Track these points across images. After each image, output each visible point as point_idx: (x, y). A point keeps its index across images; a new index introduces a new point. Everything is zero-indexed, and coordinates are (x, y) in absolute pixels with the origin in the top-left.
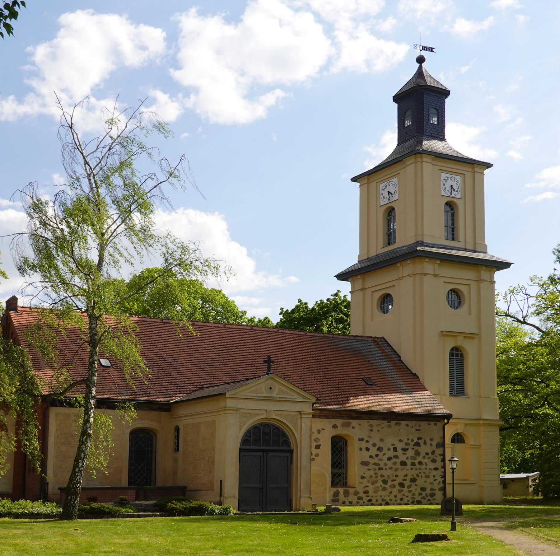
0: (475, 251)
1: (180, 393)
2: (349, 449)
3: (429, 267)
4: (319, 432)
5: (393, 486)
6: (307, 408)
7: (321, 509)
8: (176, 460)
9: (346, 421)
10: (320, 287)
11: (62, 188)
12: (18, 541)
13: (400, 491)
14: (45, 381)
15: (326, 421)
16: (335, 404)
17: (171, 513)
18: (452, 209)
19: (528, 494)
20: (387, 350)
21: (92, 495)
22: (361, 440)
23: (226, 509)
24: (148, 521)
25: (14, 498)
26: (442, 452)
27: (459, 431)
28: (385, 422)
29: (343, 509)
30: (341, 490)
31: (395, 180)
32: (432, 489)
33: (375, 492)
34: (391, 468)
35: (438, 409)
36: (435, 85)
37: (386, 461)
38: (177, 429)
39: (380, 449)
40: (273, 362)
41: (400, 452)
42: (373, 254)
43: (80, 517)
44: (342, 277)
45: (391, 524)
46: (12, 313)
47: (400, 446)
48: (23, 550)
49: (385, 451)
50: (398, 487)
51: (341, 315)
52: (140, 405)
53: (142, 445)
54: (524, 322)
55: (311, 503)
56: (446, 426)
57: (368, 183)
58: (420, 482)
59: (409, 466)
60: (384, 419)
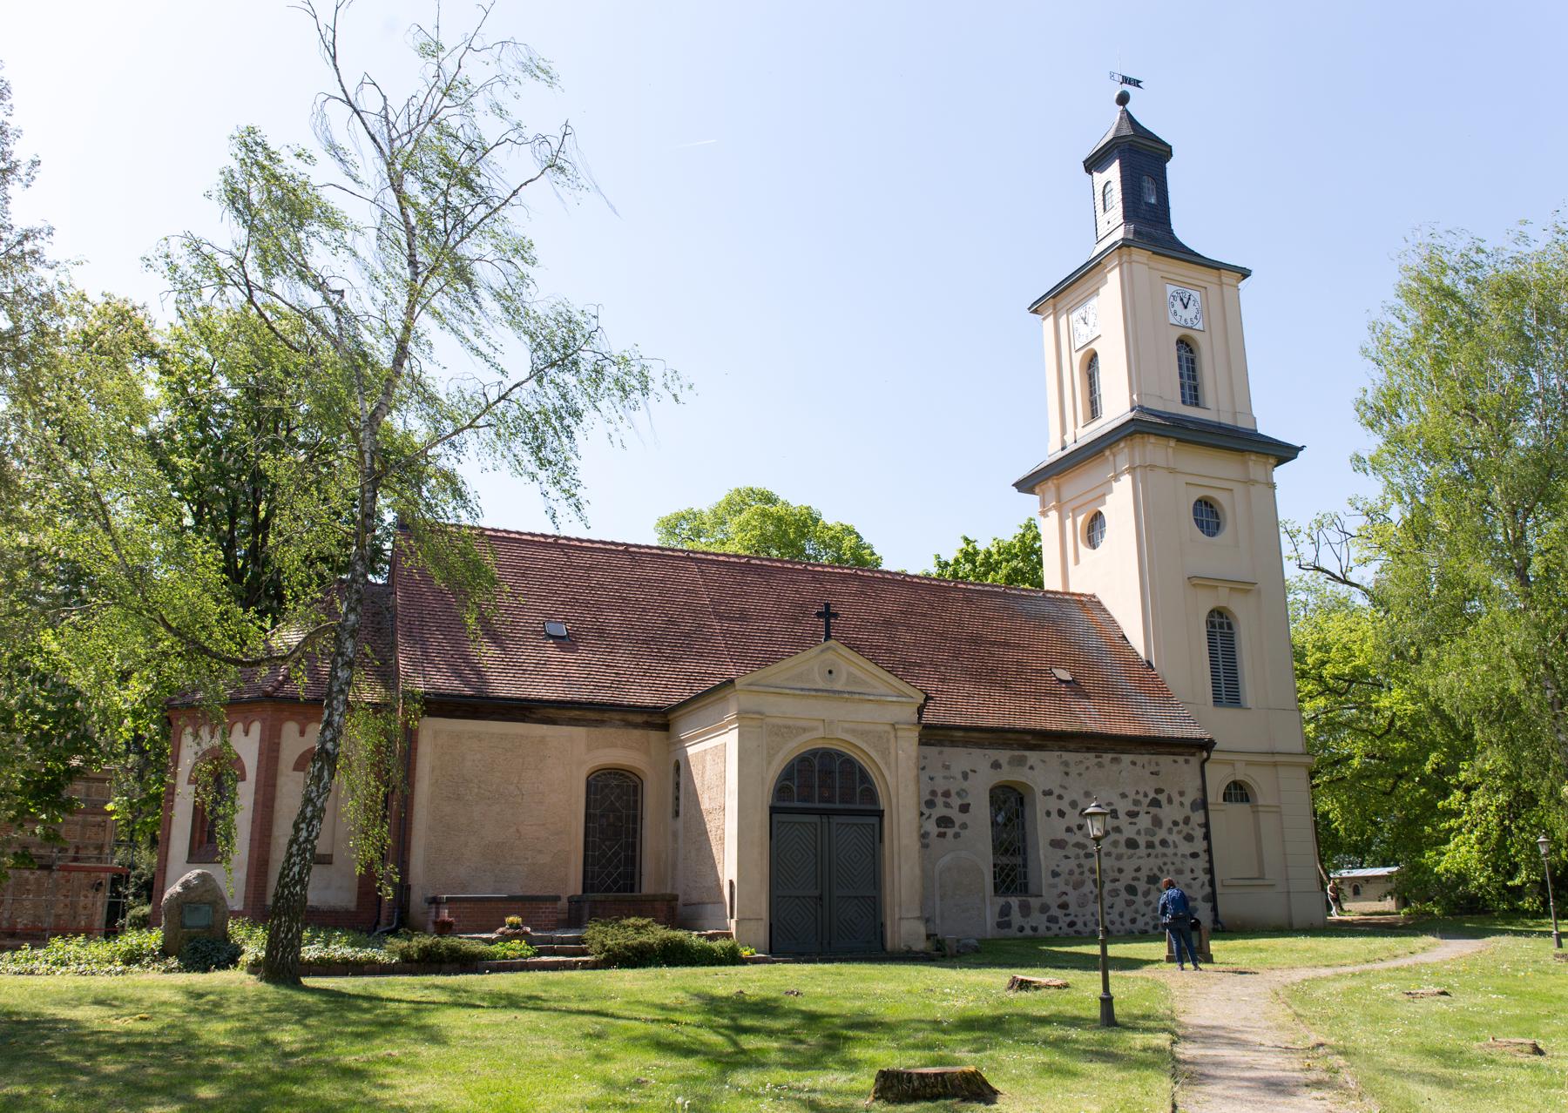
4: (965, 776)
5: (1115, 893)
9: (1016, 753)
13: (1129, 903)
22: (1048, 793)
26: (1202, 820)
28: (1091, 755)
30: (1014, 901)
33: (1081, 905)
40: (836, 615)
41: (1123, 820)
47: (1123, 807)
50: (1124, 895)
56: (1207, 765)
59: (1142, 851)
60: (1088, 750)
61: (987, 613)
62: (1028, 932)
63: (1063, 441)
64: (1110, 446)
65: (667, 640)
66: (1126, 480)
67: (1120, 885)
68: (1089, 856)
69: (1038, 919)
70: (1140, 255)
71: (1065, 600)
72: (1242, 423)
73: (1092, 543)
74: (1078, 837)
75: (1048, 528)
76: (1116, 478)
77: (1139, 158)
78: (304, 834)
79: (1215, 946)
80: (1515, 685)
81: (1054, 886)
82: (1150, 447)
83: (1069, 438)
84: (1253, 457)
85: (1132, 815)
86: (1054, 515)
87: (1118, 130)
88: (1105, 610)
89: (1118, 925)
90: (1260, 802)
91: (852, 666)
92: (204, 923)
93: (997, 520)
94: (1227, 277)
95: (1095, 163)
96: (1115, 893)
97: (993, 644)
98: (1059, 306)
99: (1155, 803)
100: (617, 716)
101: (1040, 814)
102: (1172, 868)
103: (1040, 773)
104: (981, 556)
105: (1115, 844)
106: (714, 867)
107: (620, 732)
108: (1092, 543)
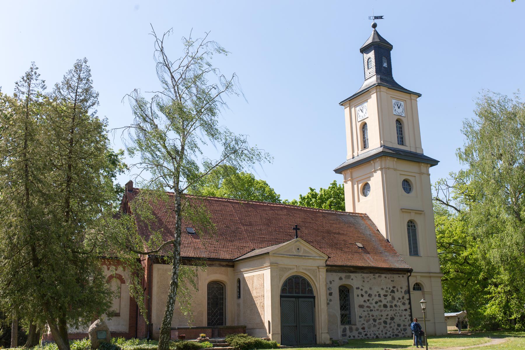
5: (380, 324)
13: (385, 327)
22: (358, 288)
26: (408, 298)
28: (372, 275)
30: (347, 327)
33: (369, 328)
40: (299, 229)
41: (382, 298)
47: (382, 293)
50: (383, 324)
56: (410, 278)
59: (389, 309)
60: (371, 273)
61: (320, 217)
62: (352, 338)
63: (353, 155)
64: (373, 160)
65: (229, 234)
66: (379, 172)
67: (382, 321)
68: (371, 310)
69: (355, 333)
70: (383, 89)
71: (354, 215)
72: (418, 152)
73: (365, 194)
74: (368, 304)
75: (348, 188)
76: (375, 172)
77: (381, 49)
78: (170, 308)
79: (428, 340)
80: (516, 253)
81: (360, 321)
82: (388, 161)
83: (355, 154)
84: (423, 164)
85: (385, 296)
86: (350, 183)
87: (374, 39)
88: (370, 220)
89: (381, 335)
90: (425, 290)
91: (305, 247)
92: (104, 337)
93: (323, 181)
94: (413, 97)
95: (364, 50)
96: (380, 324)
97: (335, 233)
98: (351, 104)
99: (393, 291)
100: (217, 263)
101: (355, 296)
102: (398, 315)
103: (355, 281)
104: (319, 196)
105: (380, 306)
106: (259, 316)
107: (218, 268)
108: (365, 194)
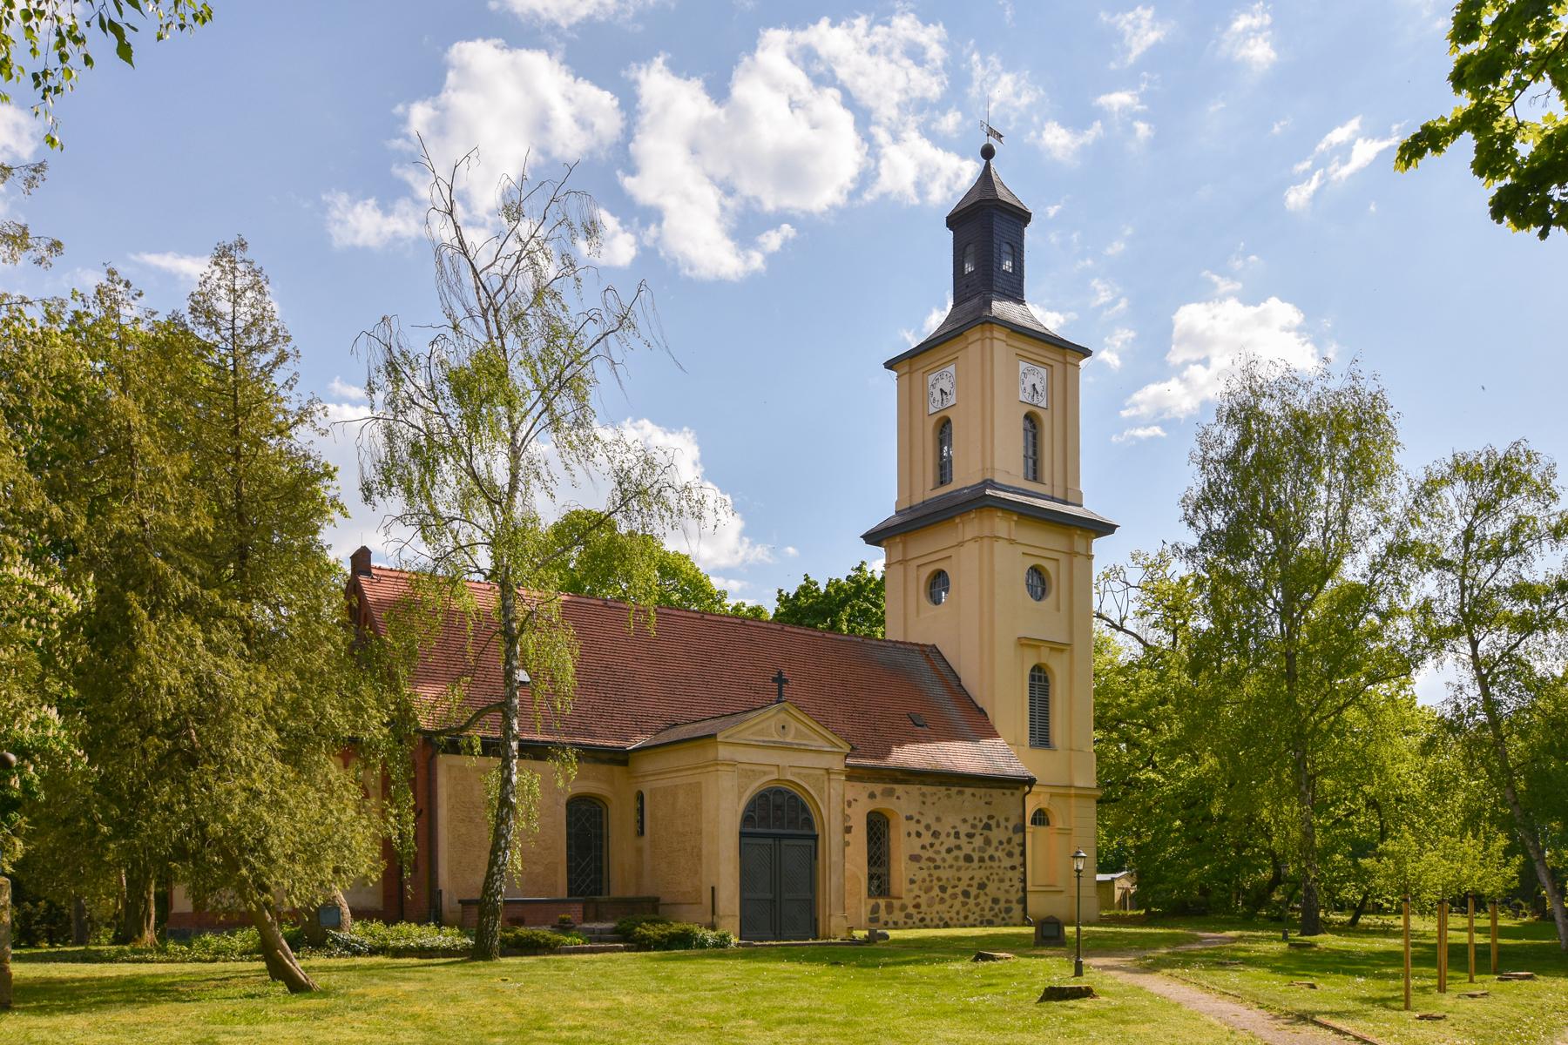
0: (1065, 502)
1: (642, 733)
2: (893, 834)
3: (1002, 525)
5: (954, 896)
6: (837, 764)
7: (860, 934)
8: (639, 851)
10: (841, 557)
11: (443, 331)
12: (417, 1009)
13: (964, 904)
14: (431, 703)
15: (859, 785)
16: (872, 758)
17: (642, 945)
18: (1034, 427)
19: (1111, 906)
20: (941, 667)
21: (519, 913)
22: (909, 818)
23: (724, 937)
24: (610, 961)
25: (390, 921)
27: (1042, 806)
28: (943, 788)
29: (893, 934)
30: (882, 902)
31: (951, 369)
32: (1007, 901)
34: (951, 867)
35: (1016, 768)
36: (1009, 200)
37: (944, 854)
38: (640, 797)
39: (936, 834)
41: (963, 840)
42: (918, 500)
43: (504, 954)
44: (872, 538)
45: (981, 964)
46: (363, 579)
47: (964, 829)
48: (431, 1029)
49: (943, 837)
50: (961, 898)
51: (866, 605)
52: (590, 755)
53: (586, 822)
54: (1120, 628)
55: (846, 925)
57: (910, 373)
58: (992, 888)
59: (976, 864)
60: (941, 784)
67: (958, 891)
85: (970, 836)
